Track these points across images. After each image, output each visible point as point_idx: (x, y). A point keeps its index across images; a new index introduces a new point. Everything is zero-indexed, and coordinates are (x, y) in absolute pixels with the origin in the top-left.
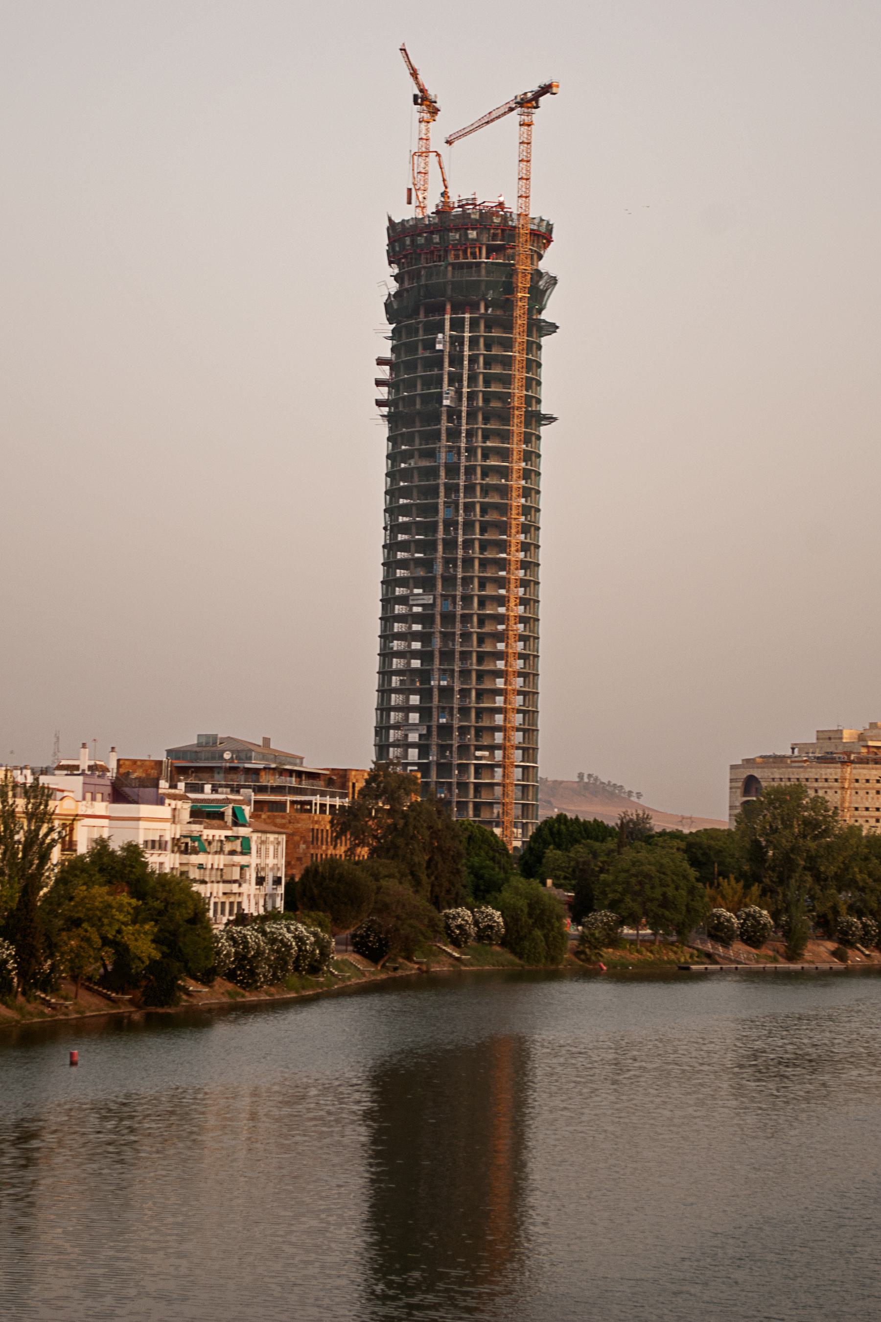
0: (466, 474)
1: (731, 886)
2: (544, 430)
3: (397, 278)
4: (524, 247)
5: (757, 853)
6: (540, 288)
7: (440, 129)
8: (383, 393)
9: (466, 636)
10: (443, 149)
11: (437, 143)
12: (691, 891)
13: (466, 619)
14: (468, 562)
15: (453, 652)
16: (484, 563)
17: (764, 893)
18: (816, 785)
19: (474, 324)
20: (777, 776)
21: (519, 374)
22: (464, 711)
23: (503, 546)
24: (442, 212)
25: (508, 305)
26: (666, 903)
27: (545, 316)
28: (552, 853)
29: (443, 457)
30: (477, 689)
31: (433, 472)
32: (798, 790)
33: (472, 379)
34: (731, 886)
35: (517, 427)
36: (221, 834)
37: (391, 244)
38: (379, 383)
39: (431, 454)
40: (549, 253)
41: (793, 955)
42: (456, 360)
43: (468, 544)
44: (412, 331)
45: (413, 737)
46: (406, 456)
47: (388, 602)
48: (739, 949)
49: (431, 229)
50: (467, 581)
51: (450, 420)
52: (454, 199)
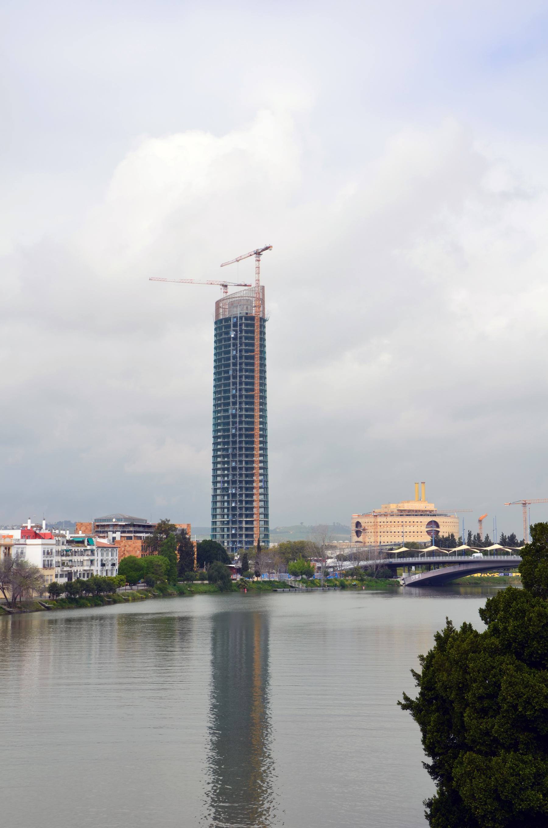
0: (239, 417)
15: (236, 481)
18: (380, 524)
20: (367, 521)
29: (231, 373)
30: (245, 494)
36: (82, 549)
51: (233, 359)
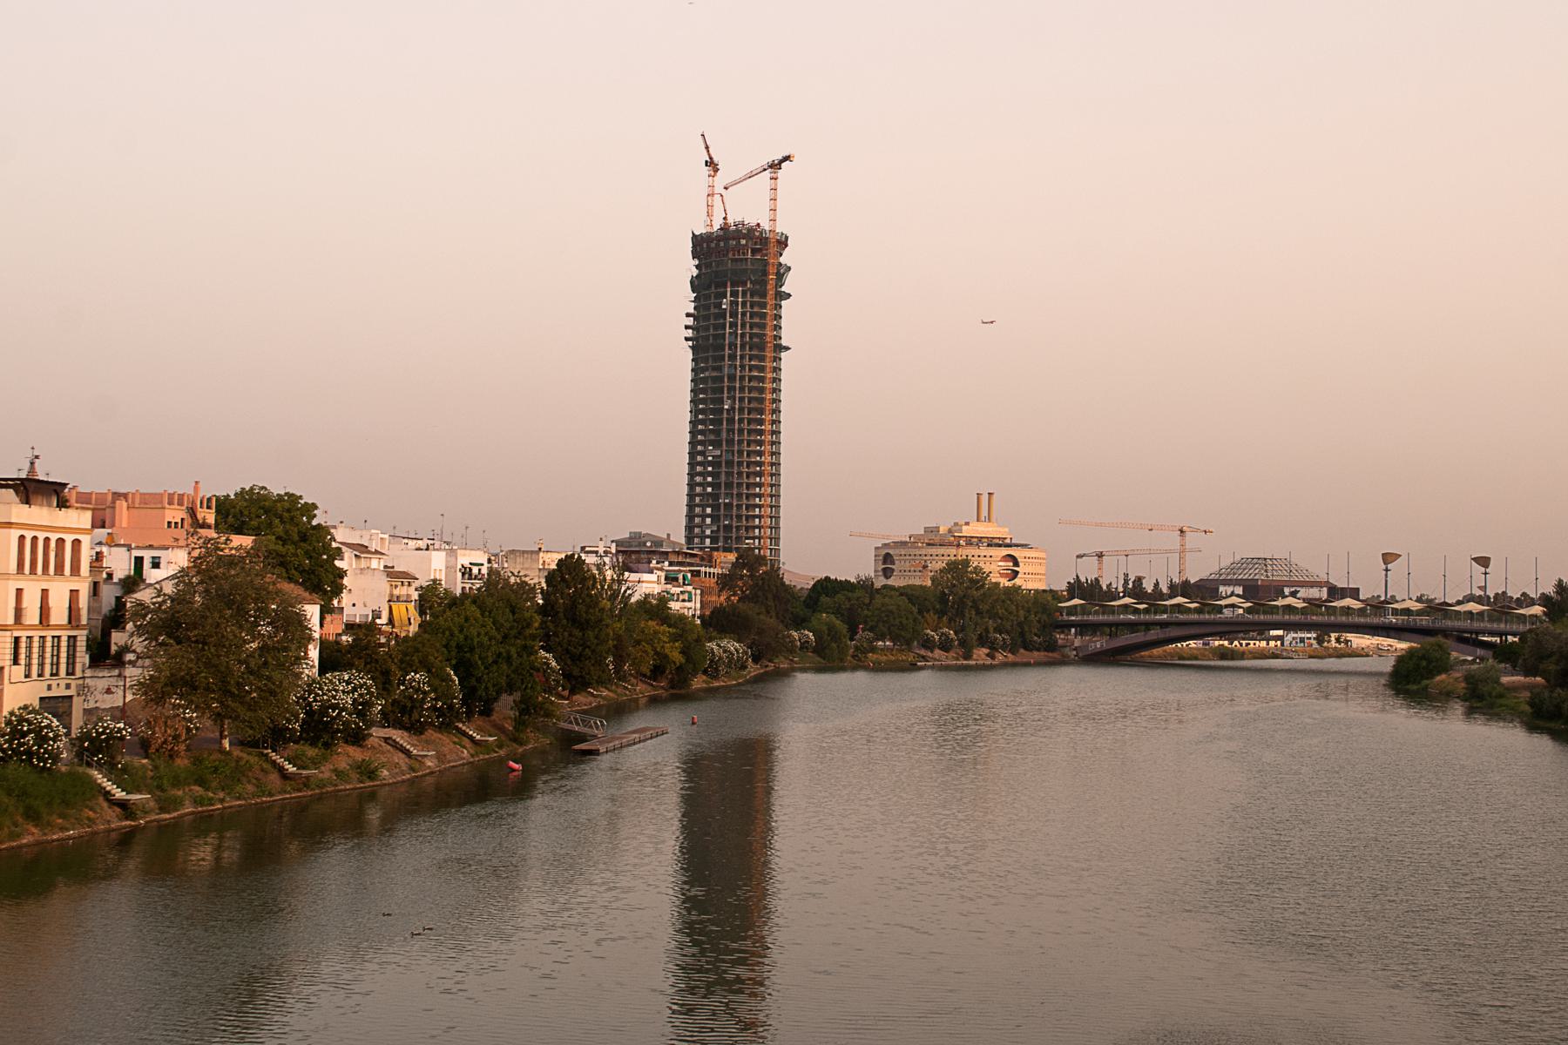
1: (931, 617)
2: (783, 355)
3: (697, 267)
4: (773, 249)
5: (943, 598)
6: (782, 273)
7: (721, 179)
8: (690, 333)
9: (740, 474)
10: (723, 192)
11: (719, 189)
12: (915, 620)
13: (740, 464)
14: (741, 431)
16: (750, 432)
17: (950, 620)
19: (744, 293)
21: (770, 323)
22: (739, 517)
23: (761, 422)
24: (725, 228)
25: (764, 283)
26: (902, 627)
27: (783, 289)
28: (824, 599)
31: (721, 379)
32: (966, 562)
33: (743, 326)
34: (931, 617)
35: (769, 354)
36: (678, 590)
37: (694, 246)
38: (687, 327)
39: (720, 369)
40: (786, 252)
41: (968, 656)
42: (734, 314)
43: (741, 421)
44: (708, 297)
45: (708, 532)
46: (703, 370)
47: (692, 454)
48: (938, 653)
49: (719, 239)
50: (740, 442)
52: (731, 221)
